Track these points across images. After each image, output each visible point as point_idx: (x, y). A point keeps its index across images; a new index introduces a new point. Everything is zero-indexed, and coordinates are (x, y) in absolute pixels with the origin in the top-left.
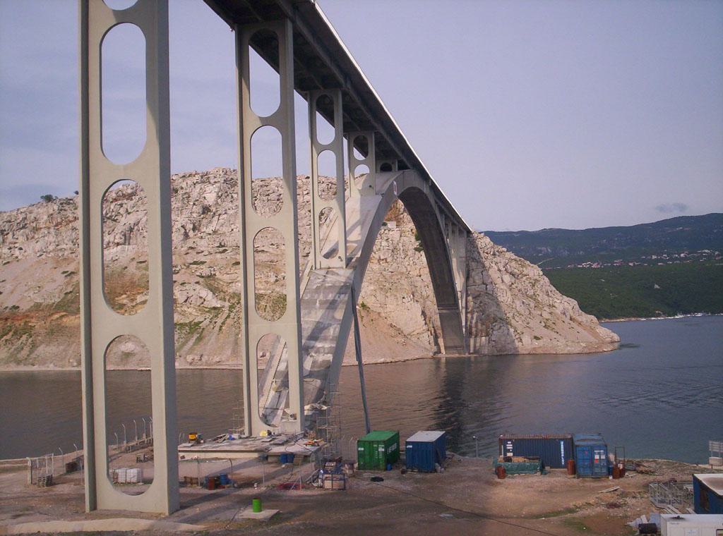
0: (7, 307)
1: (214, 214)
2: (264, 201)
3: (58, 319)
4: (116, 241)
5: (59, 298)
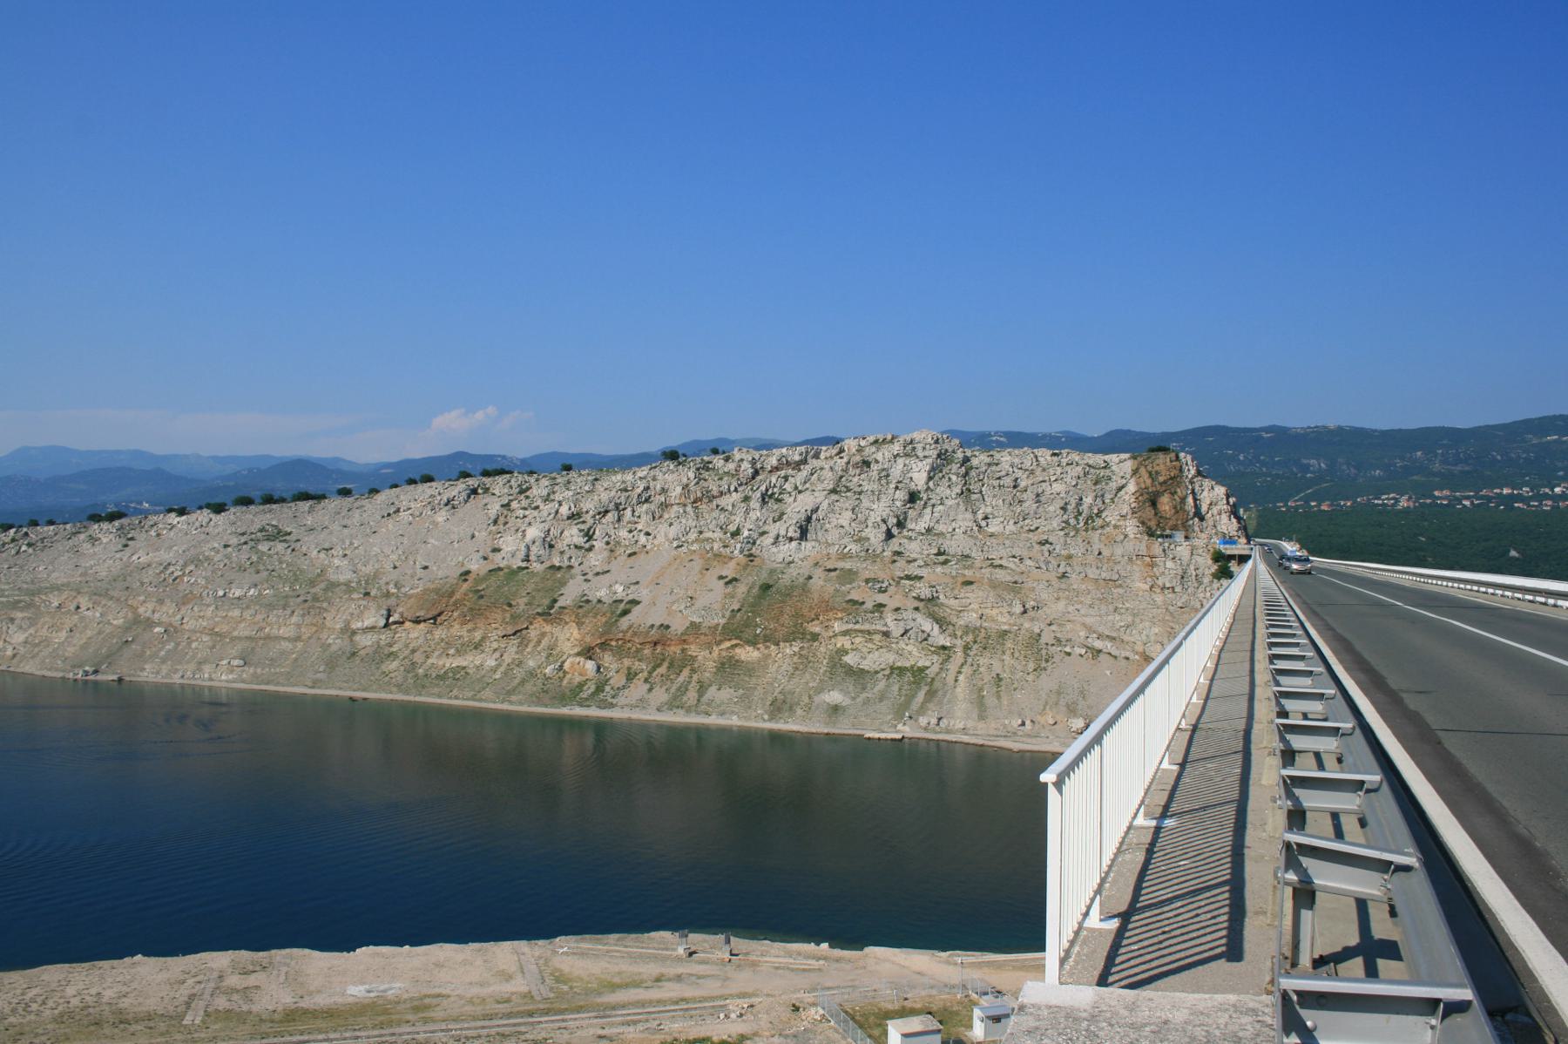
0: (652, 626)
1: (926, 503)
2: (994, 487)
3: (728, 648)
4: (789, 535)
5: (723, 616)
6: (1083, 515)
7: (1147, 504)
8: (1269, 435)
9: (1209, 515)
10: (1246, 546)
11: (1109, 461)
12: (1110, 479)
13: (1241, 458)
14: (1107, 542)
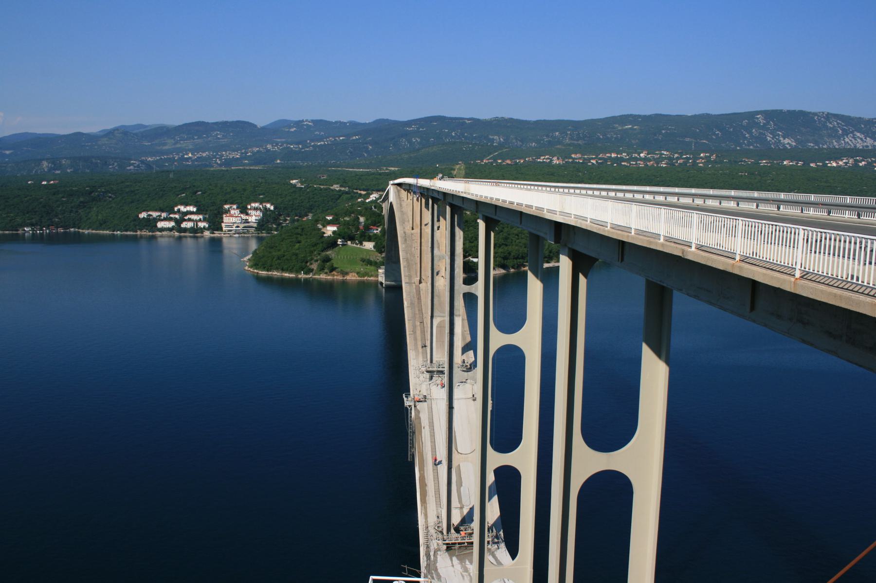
13: (453, 135)
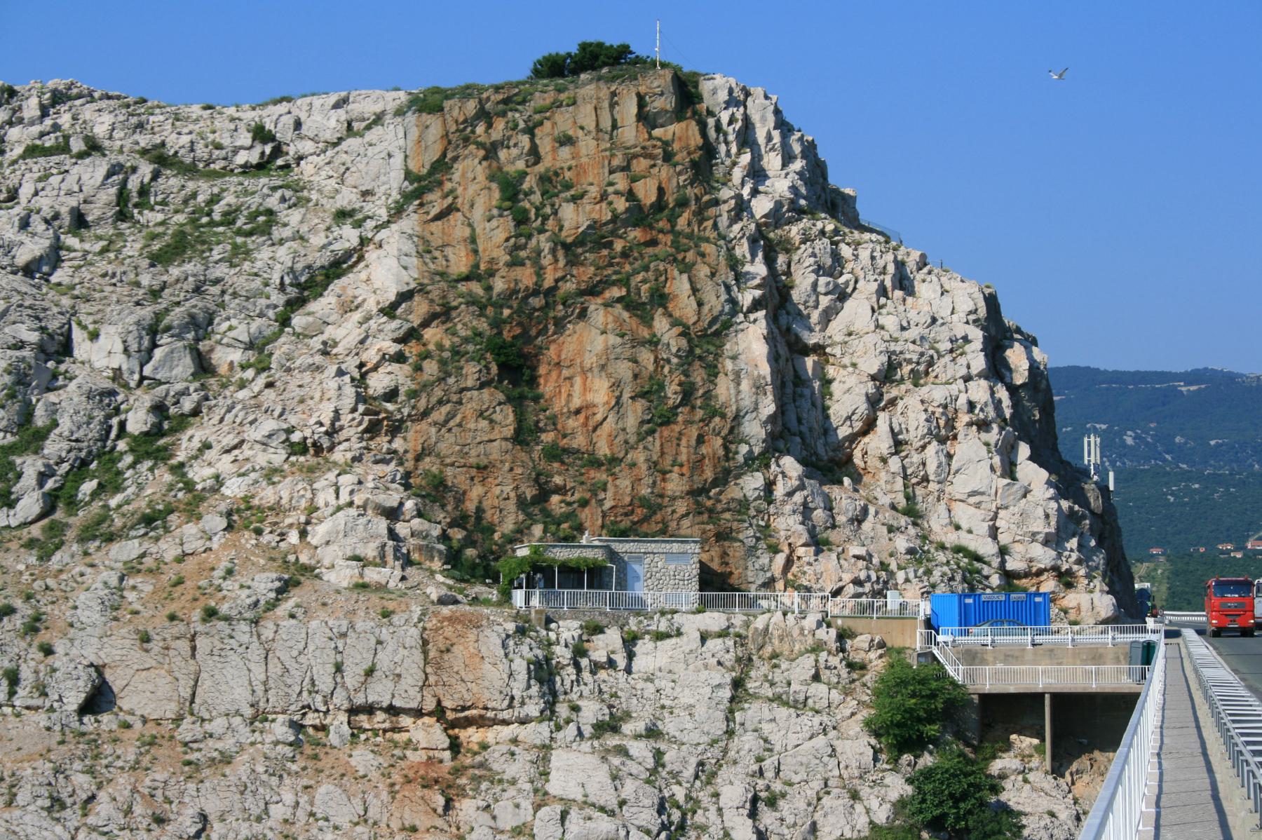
6: (54, 447)
7: (471, 371)
8: (1192, 388)
9: (879, 441)
10: (1111, 638)
11: (284, 132)
12: (265, 230)
13: (1129, 441)
14: (156, 623)
